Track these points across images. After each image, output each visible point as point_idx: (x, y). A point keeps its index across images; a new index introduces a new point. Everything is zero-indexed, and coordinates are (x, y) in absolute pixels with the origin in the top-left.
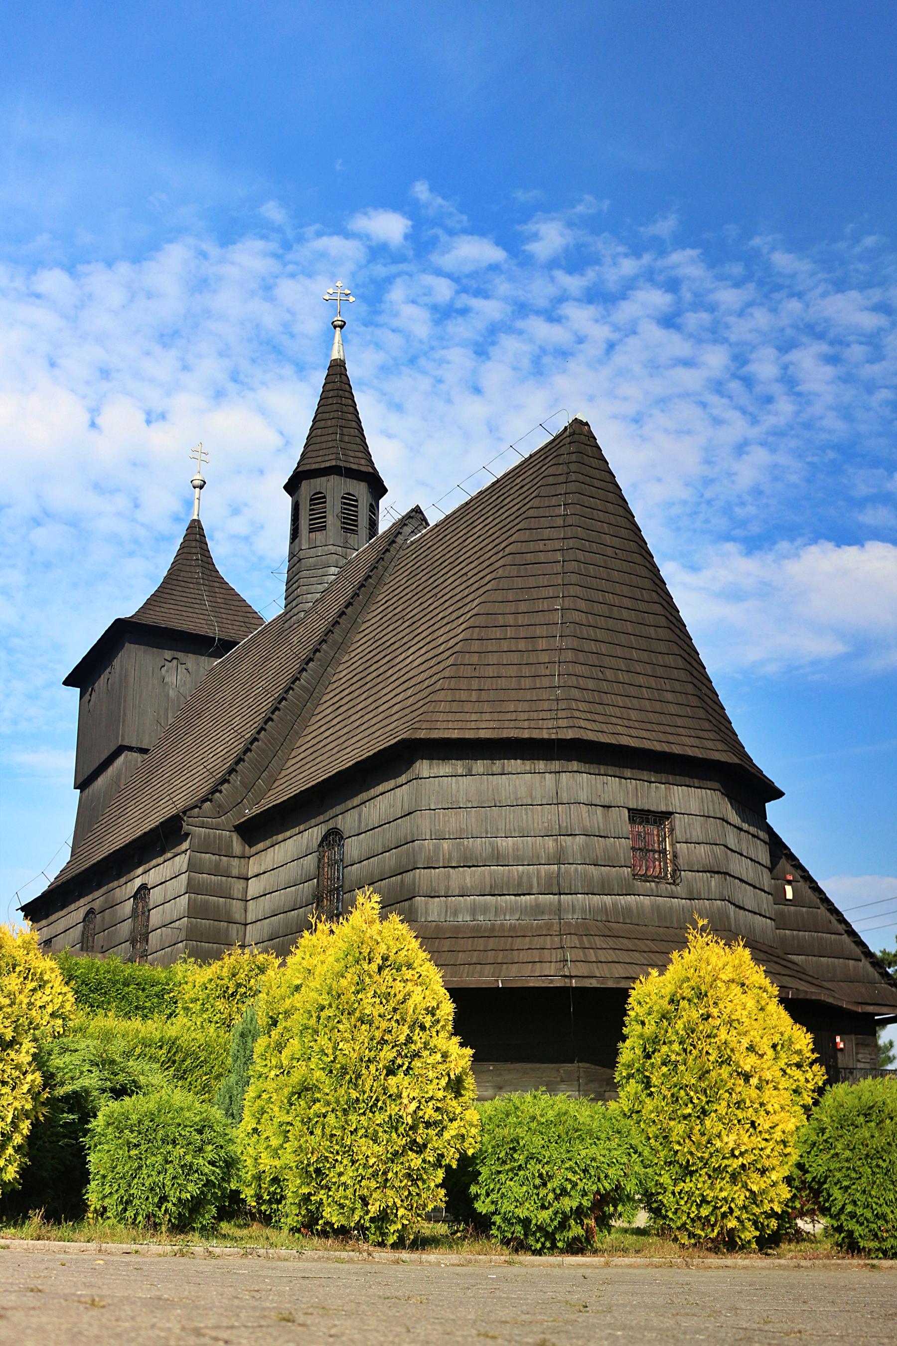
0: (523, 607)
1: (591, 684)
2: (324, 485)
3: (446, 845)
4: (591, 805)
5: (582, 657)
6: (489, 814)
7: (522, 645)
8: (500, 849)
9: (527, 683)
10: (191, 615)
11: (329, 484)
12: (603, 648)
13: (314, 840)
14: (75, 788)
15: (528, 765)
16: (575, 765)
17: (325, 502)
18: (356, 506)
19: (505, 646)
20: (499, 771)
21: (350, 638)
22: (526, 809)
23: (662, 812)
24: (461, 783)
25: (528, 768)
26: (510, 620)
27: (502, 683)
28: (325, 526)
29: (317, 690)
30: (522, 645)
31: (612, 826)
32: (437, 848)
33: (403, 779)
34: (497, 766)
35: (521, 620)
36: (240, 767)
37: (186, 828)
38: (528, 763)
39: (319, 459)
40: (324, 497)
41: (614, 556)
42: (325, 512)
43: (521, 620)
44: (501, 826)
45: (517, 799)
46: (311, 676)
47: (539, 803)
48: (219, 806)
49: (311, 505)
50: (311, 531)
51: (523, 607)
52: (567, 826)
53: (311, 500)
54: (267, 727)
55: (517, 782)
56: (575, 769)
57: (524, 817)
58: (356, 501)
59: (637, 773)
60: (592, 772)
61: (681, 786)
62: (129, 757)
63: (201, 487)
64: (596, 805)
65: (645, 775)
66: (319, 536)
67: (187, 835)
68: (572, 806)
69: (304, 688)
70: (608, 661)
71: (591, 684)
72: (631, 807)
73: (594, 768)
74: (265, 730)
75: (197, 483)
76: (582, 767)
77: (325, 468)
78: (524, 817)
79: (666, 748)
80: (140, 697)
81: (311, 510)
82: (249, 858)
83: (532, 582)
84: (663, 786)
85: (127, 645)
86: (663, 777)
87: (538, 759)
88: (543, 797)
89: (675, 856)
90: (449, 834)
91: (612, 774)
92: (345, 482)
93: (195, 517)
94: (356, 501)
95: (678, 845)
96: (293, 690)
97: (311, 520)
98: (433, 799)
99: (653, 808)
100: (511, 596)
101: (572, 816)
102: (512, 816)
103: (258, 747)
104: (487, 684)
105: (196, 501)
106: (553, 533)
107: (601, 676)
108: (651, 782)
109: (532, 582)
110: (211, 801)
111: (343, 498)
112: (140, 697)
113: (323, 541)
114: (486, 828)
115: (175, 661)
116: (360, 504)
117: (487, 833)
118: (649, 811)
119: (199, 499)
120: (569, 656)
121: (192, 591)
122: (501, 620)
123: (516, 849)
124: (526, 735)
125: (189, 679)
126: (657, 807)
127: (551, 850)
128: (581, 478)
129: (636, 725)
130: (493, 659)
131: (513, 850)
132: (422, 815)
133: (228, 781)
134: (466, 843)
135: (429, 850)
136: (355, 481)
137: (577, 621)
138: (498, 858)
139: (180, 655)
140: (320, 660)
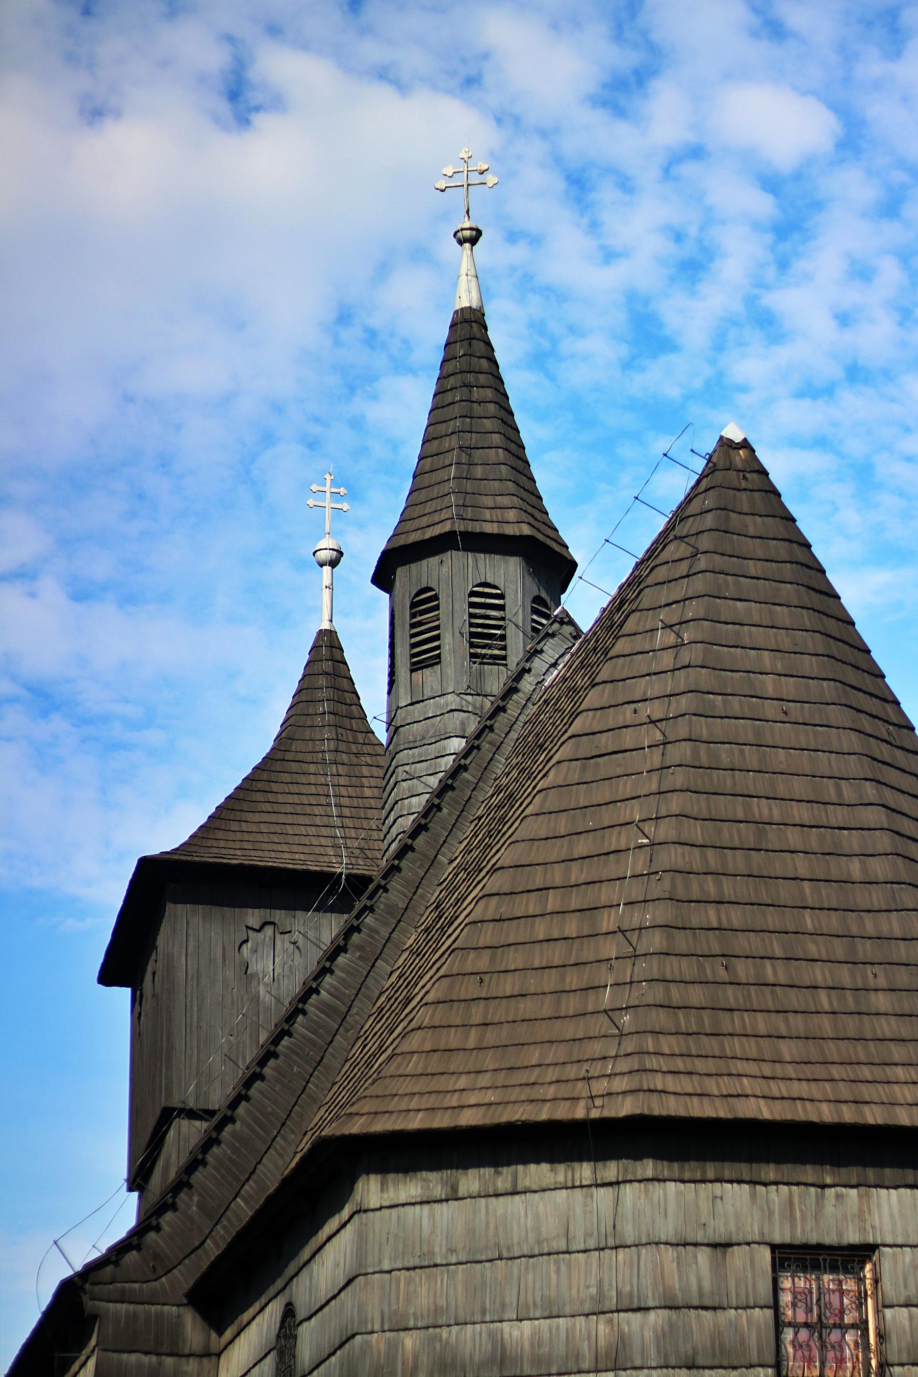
0: (582, 847)
1: (696, 995)
2: (435, 573)
3: (409, 1341)
4: (685, 1245)
5: (682, 942)
6: (488, 1274)
7: (572, 927)
8: (508, 1346)
9: (571, 1004)
10: (303, 830)
11: (445, 570)
12: (735, 916)
13: (273, 1326)
14: (130, 1189)
15: (560, 1173)
16: (648, 1167)
17: (437, 608)
18: (501, 608)
19: (541, 929)
20: (509, 1187)
21: (422, 897)
22: (557, 1262)
23: (852, 1247)
24: (438, 1218)
25: (561, 1178)
26: (557, 875)
27: (526, 1007)
28: (439, 656)
29: (354, 1010)
30: (572, 927)
31: (732, 1284)
32: (393, 1348)
33: (346, 1213)
34: (504, 1178)
35: (577, 873)
36: (198, 1177)
37: (90, 1305)
38: (561, 1168)
39: (424, 521)
40: (436, 598)
41: (782, 717)
42: (437, 628)
43: (577, 873)
44: (511, 1298)
45: (539, 1242)
46: (343, 981)
47: (582, 1247)
48: (156, 1256)
49: (413, 616)
50: (415, 667)
51: (582, 847)
52: (631, 1292)
53: (413, 605)
54: (252, 1092)
55: (541, 1209)
56: (649, 1174)
57: (554, 1277)
58: (501, 596)
59: (788, 1171)
60: (687, 1176)
61: (896, 1187)
62: (184, 1129)
63: (333, 563)
64: (696, 1245)
65: (809, 1173)
66: (429, 676)
67: (95, 1317)
68: (643, 1251)
69: (327, 1009)
70: (743, 943)
71: (696, 995)
72: (777, 1239)
73: (692, 1169)
74: (247, 1098)
75: (324, 555)
76: (665, 1168)
77: (432, 539)
78: (554, 1277)
79: (848, 1115)
80: (200, 1008)
81: (413, 626)
82: (219, 1355)
83: (603, 793)
84: (854, 1192)
85: (170, 907)
86: (853, 1173)
87: (580, 1160)
88: (587, 1235)
89: (881, 1336)
90: (416, 1319)
91: (734, 1176)
92: (476, 561)
93: (326, 626)
94: (501, 596)
95: (888, 1312)
96: (304, 1012)
97: (414, 646)
98: (387, 1251)
99: (830, 1239)
100: (562, 824)
101: (642, 1269)
102: (530, 1277)
103: (233, 1134)
104: (497, 1012)
105: (327, 592)
106: (655, 686)
107: (723, 975)
108: (823, 1186)
109: (603, 793)
110: (138, 1248)
111: (473, 594)
112: (200, 1008)
113: (437, 686)
114: (484, 1303)
115: (269, 930)
116: (508, 602)
117: (484, 1313)
118: (820, 1247)
119: (330, 587)
120: (655, 941)
121: (312, 779)
122: (538, 878)
123: (536, 1341)
124: (544, 1114)
125: (298, 960)
126: (840, 1234)
127: (602, 1342)
128: (719, 561)
129: (790, 1071)
130: (514, 959)
131: (532, 1344)
132: (366, 1284)
133: (173, 1207)
134: (445, 1335)
135: (379, 1353)
136: (497, 557)
137: (681, 865)
138: (502, 1361)
139: (278, 915)
140: (359, 948)
